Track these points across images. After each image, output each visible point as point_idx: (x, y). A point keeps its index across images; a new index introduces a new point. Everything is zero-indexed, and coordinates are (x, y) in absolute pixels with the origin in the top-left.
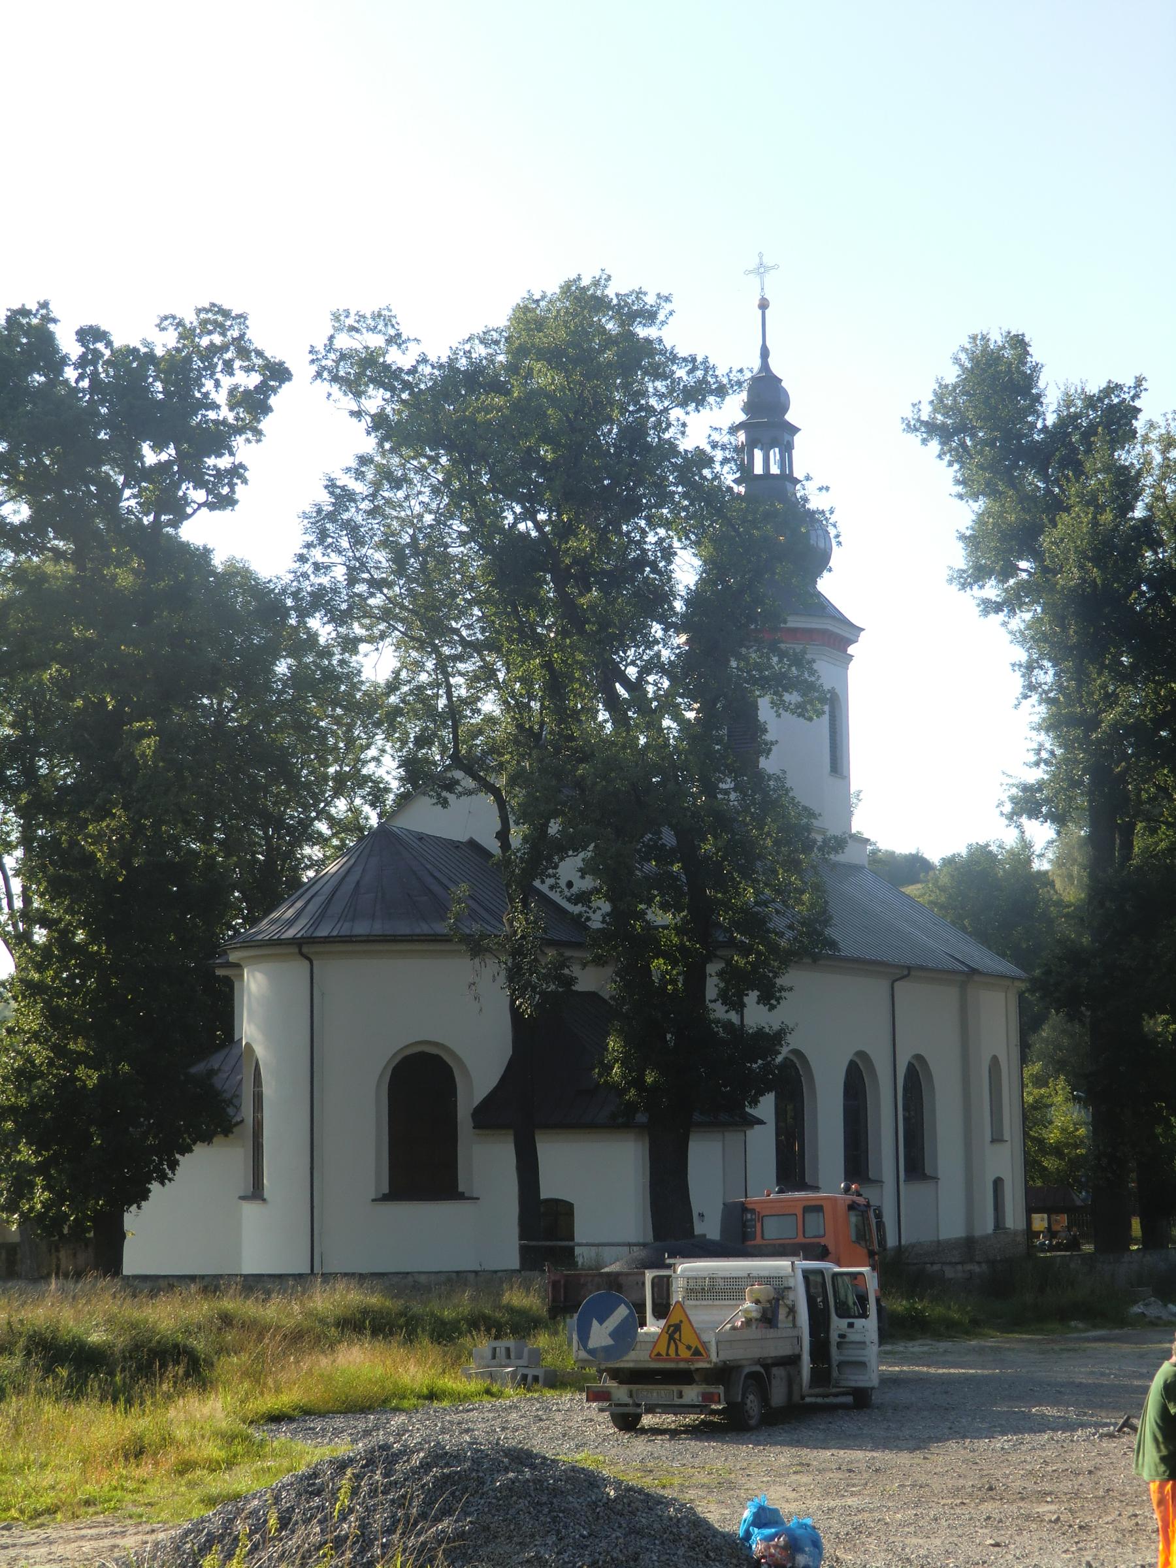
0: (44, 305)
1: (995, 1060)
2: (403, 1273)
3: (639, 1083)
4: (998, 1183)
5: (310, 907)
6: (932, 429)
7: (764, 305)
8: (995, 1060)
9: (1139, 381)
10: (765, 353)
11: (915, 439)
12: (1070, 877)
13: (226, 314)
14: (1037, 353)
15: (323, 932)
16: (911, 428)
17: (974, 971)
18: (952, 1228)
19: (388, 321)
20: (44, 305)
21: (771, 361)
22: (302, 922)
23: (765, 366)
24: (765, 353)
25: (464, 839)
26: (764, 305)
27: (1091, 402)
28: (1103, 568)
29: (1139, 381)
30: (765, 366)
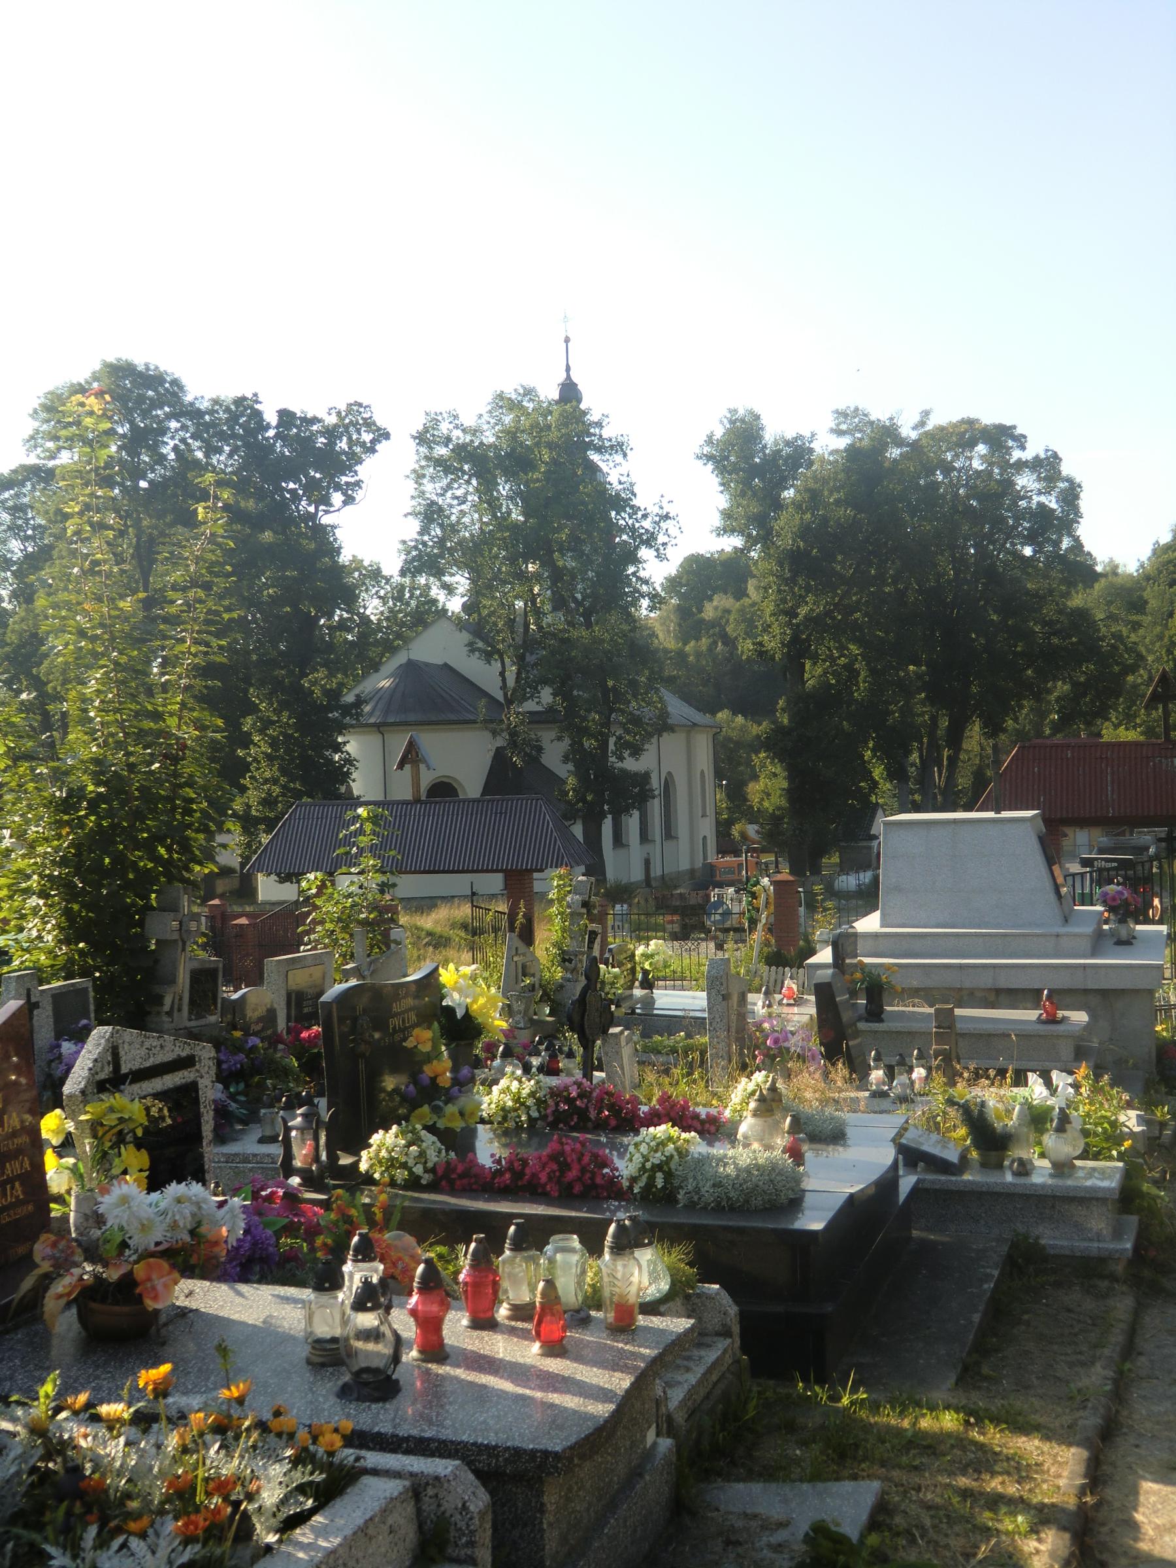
0: (255, 395)
1: (702, 772)
2: (431, 898)
3: (584, 800)
4: (705, 838)
5: (379, 706)
6: (709, 458)
7: (567, 340)
8: (702, 772)
9: (813, 435)
10: (568, 369)
11: (700, 462)
12: (669, 632)
13: (360, 405)
14: (764, 421)
15: (391, 720)
16: (699, 457)
17: (695, 724)
18: (684, 865)
19: (456, 417)
20: (255, 395)
21: (571, 373)
22: (377, 713)
23: (568, 376)
24: (568, 369)
25: (440, 663)
26: (567, 340)
27: (788, 443)
28: (805, 541)
29: (813, 435)
30: (568, 376)
